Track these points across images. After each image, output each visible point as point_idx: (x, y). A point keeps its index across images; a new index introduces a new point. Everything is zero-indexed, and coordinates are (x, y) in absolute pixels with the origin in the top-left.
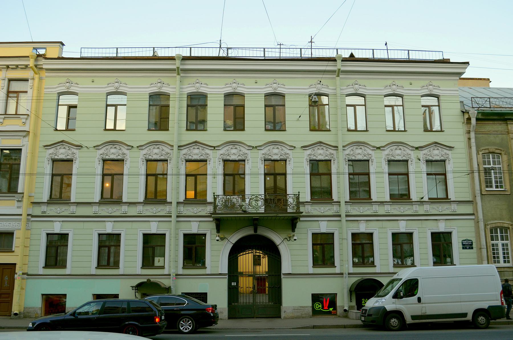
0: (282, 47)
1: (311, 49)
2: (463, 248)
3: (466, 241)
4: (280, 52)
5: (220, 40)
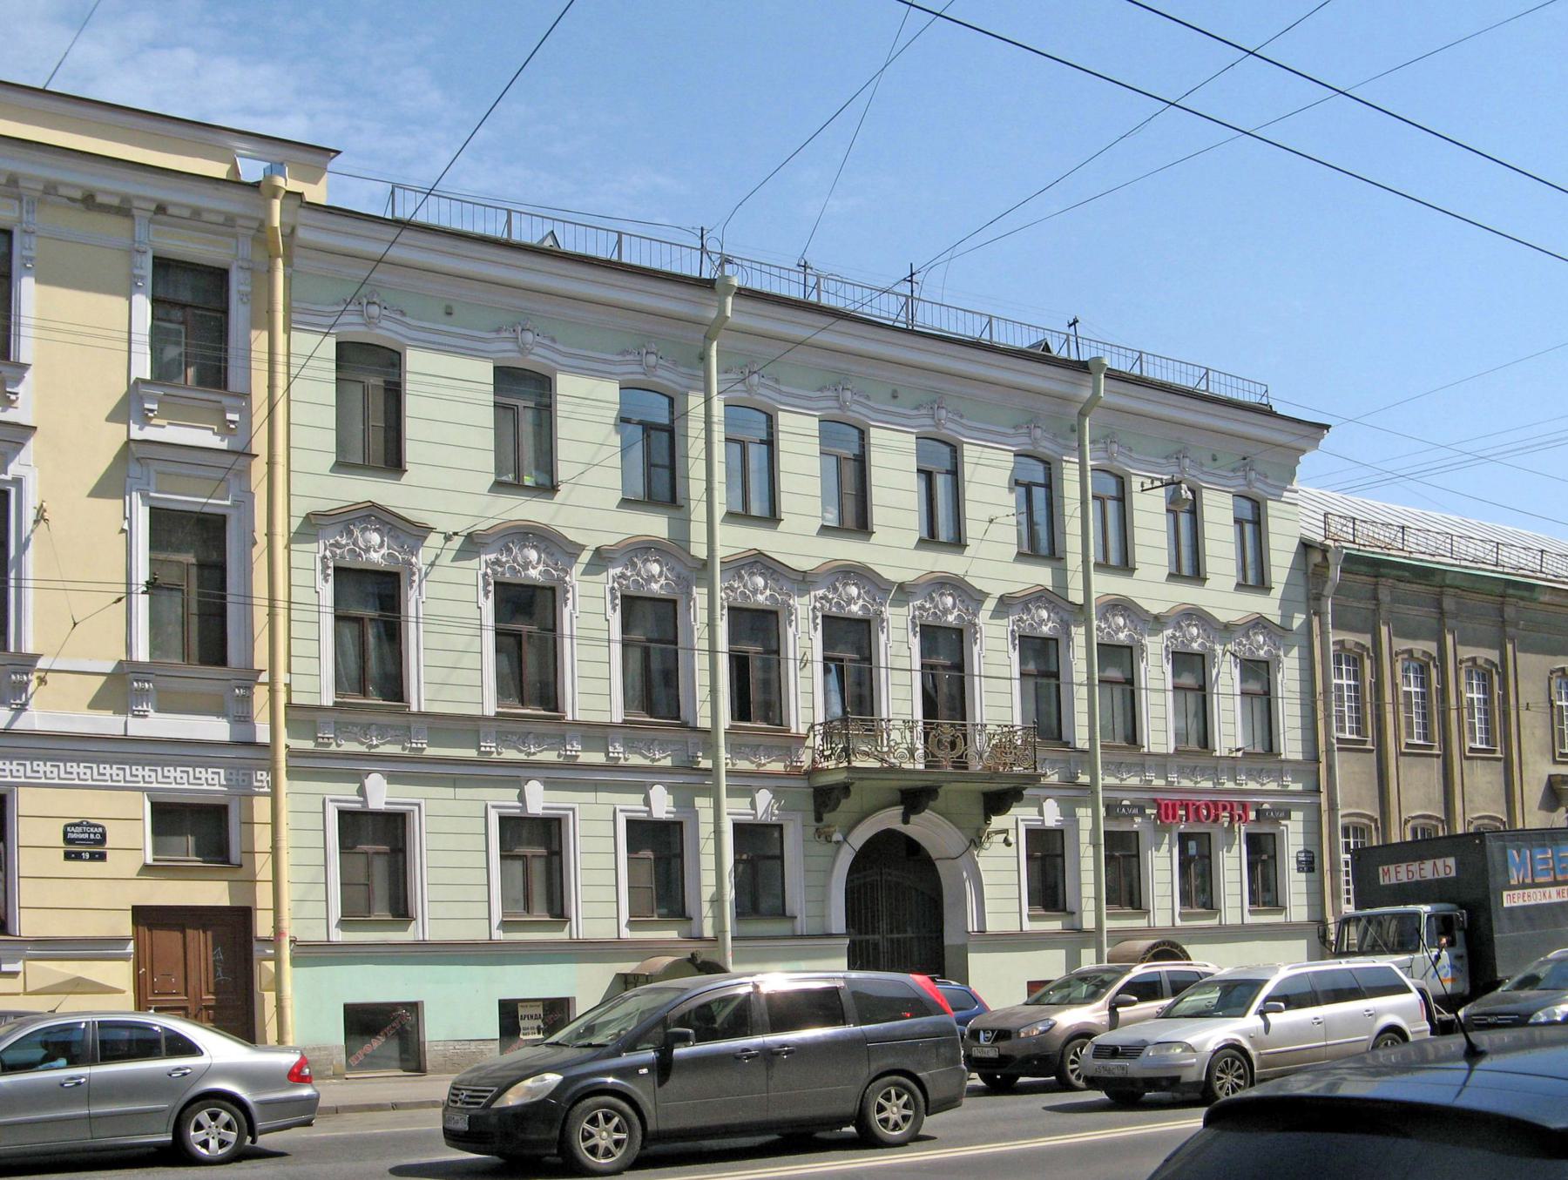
2: (68, 856)
3: (79, 829)
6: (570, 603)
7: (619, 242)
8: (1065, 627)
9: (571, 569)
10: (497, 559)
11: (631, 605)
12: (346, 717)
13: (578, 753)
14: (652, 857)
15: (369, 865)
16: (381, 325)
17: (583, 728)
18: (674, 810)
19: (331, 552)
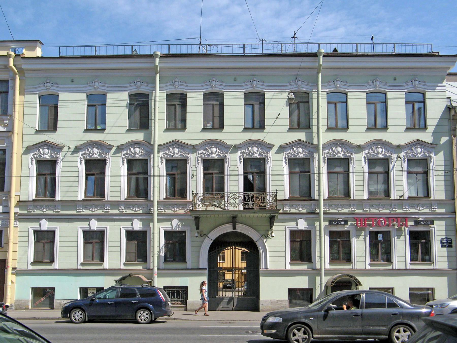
0: (264, 42)
1: (198, 46)
4: (262, 49)
5: (200, 37)
6: (432, 162)
7: (394, 47)
8: (312, 154)
10: (368, 152)
11: (131, 163)
13: (109, 210)
14: (136, 242)
15: (44, 246)
16: (141, 88)
17: (110, 202)
18: (142, 227)
19: (367, 155)
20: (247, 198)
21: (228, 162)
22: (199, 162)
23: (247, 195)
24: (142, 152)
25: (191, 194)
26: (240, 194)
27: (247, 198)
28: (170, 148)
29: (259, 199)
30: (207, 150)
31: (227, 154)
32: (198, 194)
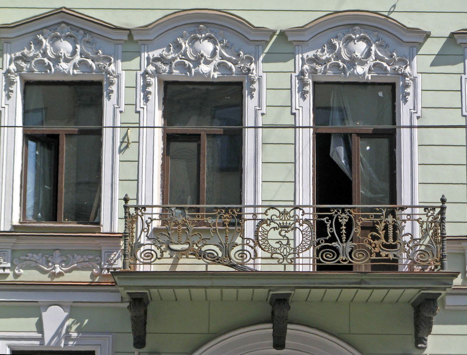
9: (412, 59)
10: (316, 56)
12: (24, 244)
20: (331, 226)
21: (256, 94)
22: (150, 93)
23: (331, 217)
24: (222, 57)
25: (119, 211)
26: (304, 213)
27: (331, 226)
28: (41, 37)
29: (377, 231)
30: (178, 47)
31: (253, 66)
32: (144, 208)
